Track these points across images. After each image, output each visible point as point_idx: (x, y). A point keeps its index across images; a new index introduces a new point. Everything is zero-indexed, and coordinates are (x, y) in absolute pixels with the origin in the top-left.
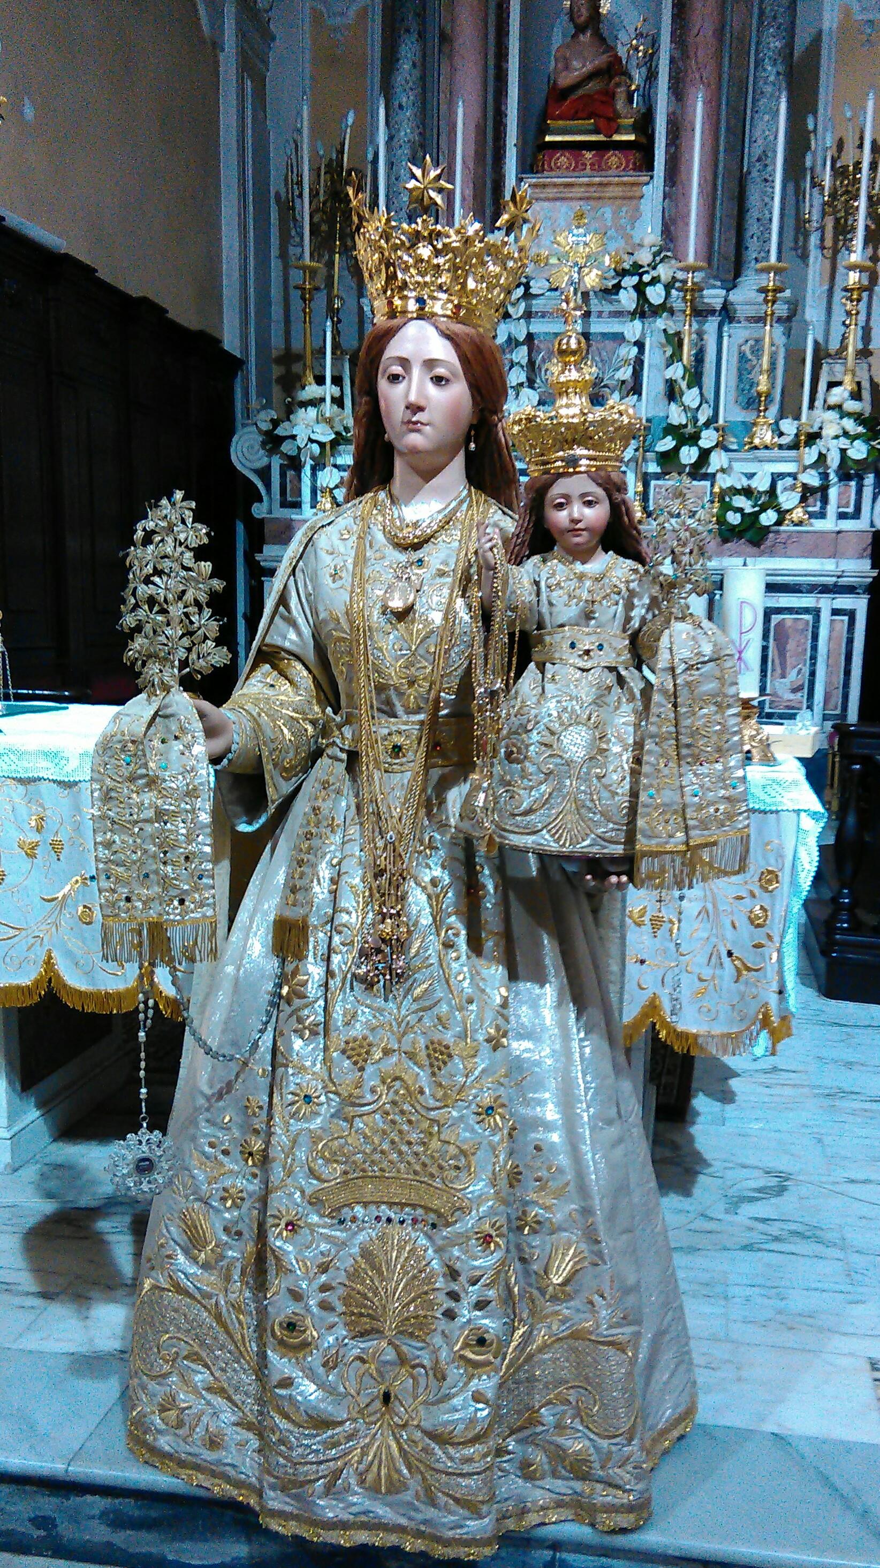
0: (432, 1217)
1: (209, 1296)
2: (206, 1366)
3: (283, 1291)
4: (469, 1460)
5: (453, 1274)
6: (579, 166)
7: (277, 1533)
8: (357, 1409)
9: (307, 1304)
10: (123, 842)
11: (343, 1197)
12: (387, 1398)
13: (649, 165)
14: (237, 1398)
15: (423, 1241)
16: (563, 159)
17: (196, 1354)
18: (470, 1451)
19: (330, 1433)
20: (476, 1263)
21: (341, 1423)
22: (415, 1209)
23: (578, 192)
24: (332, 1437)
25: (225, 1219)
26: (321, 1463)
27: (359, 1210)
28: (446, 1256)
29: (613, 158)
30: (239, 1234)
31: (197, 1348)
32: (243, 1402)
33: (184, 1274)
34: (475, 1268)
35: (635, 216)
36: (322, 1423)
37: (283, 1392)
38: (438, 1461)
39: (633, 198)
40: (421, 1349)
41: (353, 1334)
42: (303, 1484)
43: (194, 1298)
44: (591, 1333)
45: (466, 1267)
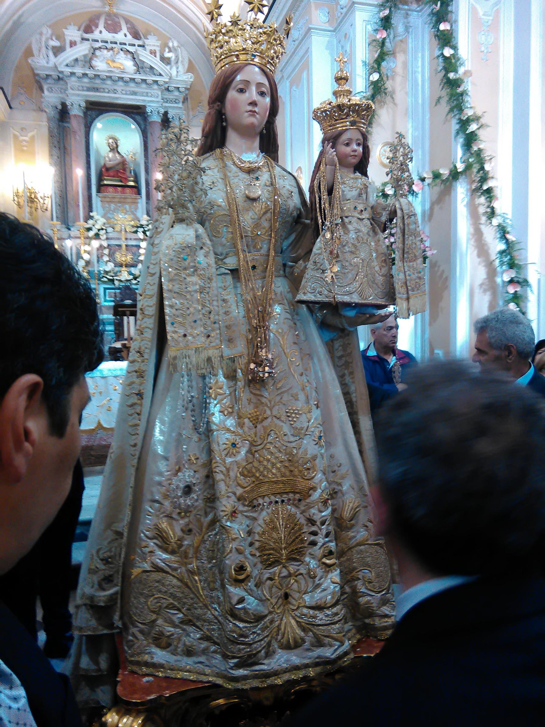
0: (297, 496)
1: (175, 569)
2: (179, 610)
3: (234, 550)
4: (336, 614)
5: (312, 522)
6: (117, 192)
7: (243, 689)
8: (272, 606)
9: (245, 555)
10: (181, 304)
11: (254, 495)
12: (286, 596)
13: (139, 193)
14: (198, 624)
15: (293, 510)
16: (111, 189)
17: (172, 604)
18: (335, 610)
19: (263, 623)
20: (323, 514)
21: (265, 616)
22: (288, 495)
23: (116, 200)
24: (264, 624)
25: (181, 524)
26: (262, 640)
27: (261, 501)
28: (307, 515)
29: (128, 190)
30: (190, 531)
31: (171, 601)
32: (203, 625)
33: (160, 559)
34: (324, 516)
35: (136, 208)
36: (259, 618)
37: (240, 606)
38: (321, 620)
39: (135, 203)
40: (299, 565)
41: (265, 566)
42: (255, 655)
43: (167, 573)
44: (367, 540)
45: (319, 517)
